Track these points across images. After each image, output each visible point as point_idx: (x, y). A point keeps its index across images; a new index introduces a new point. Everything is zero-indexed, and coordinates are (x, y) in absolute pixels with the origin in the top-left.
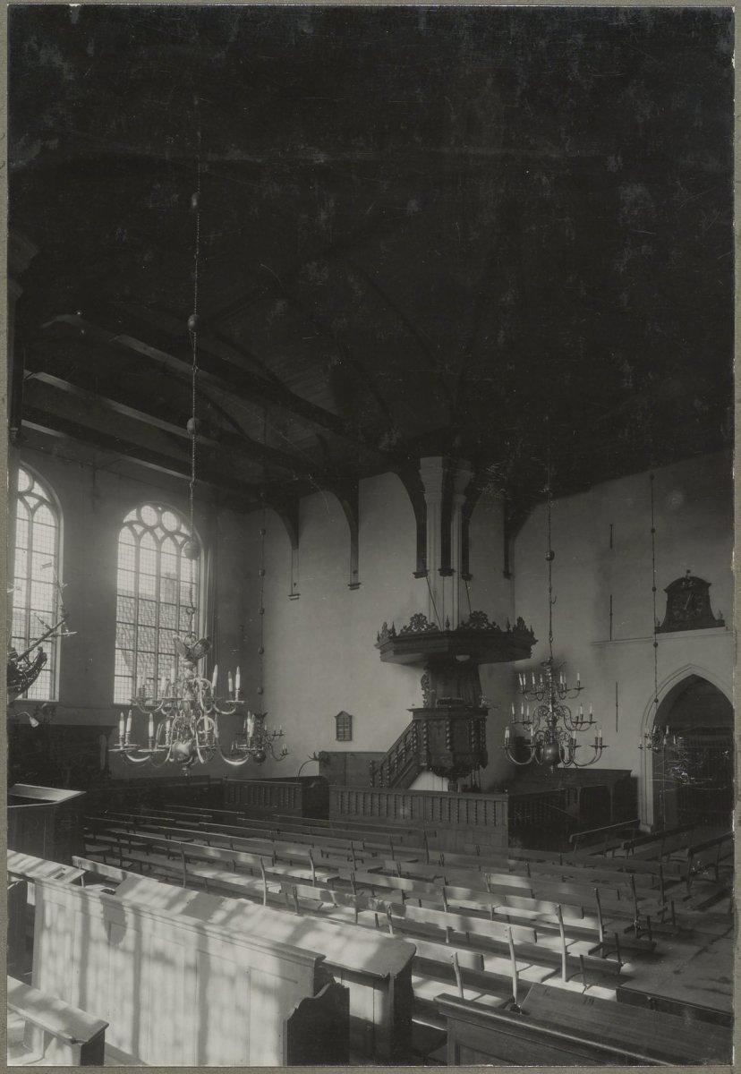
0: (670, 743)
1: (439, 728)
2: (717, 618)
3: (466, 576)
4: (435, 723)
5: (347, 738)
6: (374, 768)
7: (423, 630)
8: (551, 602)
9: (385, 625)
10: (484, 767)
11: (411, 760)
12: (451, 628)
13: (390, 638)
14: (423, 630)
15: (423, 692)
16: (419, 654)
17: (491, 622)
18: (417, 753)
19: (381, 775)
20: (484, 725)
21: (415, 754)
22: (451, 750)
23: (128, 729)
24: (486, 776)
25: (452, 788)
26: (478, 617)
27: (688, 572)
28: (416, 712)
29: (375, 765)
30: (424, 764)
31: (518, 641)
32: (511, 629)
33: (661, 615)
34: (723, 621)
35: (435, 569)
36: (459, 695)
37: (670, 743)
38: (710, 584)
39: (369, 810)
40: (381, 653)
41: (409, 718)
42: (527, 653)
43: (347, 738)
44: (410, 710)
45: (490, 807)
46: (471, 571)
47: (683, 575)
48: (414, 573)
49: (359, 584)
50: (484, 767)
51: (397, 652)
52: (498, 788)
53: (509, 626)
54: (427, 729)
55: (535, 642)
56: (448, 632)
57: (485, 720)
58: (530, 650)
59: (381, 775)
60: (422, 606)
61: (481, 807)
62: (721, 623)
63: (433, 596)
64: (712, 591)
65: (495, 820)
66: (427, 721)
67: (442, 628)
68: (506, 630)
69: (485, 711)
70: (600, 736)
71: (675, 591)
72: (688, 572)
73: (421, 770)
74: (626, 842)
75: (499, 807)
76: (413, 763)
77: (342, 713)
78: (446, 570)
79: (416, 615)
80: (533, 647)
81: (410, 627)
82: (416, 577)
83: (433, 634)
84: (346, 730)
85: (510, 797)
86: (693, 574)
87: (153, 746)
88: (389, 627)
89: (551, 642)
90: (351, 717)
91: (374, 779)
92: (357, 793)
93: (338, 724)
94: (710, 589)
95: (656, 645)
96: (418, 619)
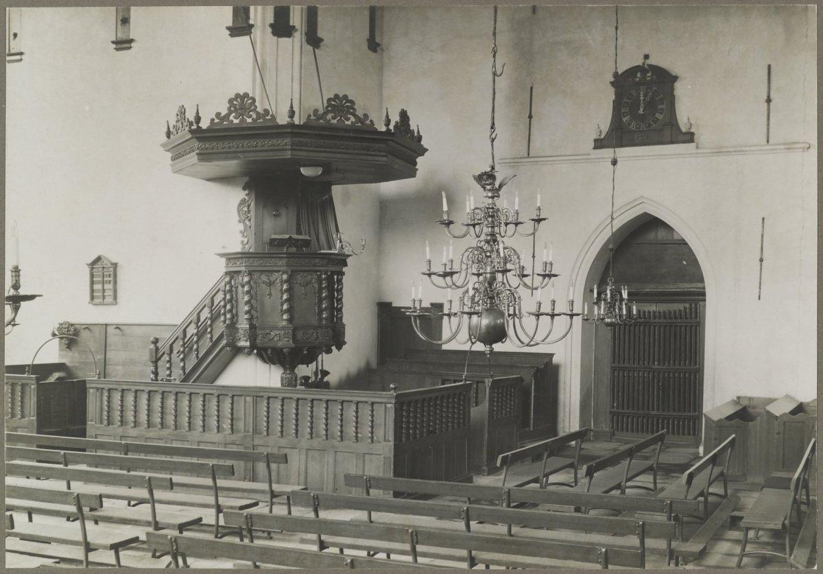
0: (629, 310)
1: (270, 284)
2: (684, 130)
3: (313, 40)
4: (264, 278)
5: (109, 299)
6: (157, 349)
7: (249, 120)
8: (495, 74)
9: (182, 111)
10: (339, 348)
11: (221, 337)
12: (296, 121)
13: (191, 131)
14: (249, 120)
15: (241, 227)
16: (235, 162)
17: (360, 113)
18: (232, 326)
19: (169, 361)
20: (340, 281)
21: (228, 327)
22: (290, 320)
23: (468, 203)
24: (338, 364)
25: (290, 382)
26: (340, 105)
27: (646, 57)
28: (230, 258)
29: (159, 345)
30: (244, 343)
31: (398, 149)
32: (391, 127)
33: (605, 125)
34: (692, 134)
35: (264, 26)
36: (299, 232)
37: (629, 310)
38: (675, 78)
39: (157, 419)
40: (173, 159)
41: (220, 267)
42: (409, 170)
43: (109, 299)
44: (222, 255)
45: (365, 411)
46: (321, 33)
47: (639, 62)
48: (228, 28)
49: (131, 41)
50: (339, 348)
51: (204, 156)
52: (359, 381)
53: (388, 122)
54: (251, 288)
55: (423, 151)
56: (292, 125)
57: (343, 274)
58: (415, 164)
59: (169, 361)
60: (243, 82)
61: (350, 413)
62: (689, 137)
63: (260, 68)
64: (680, 89)
65: (357, 433)
66: (250, 274)
67: (283, 119)
68: (384, 129)
69: (342, 260)
70: (420, 297)
71: (625, 83)
72: (646, 57)
73: (237, 351)
74: (590, 464)
75: (380, 410)
76: (224, 342)
77: (99, 259)
78: (281, 28)
79: (237, 96)
80: (419, 160)
81: (228, 115)
82: (232, 35)
83: (267, 130)
84: (106, 286)
85: (397, 397)
86: (652, 61)
87: (628, 408)
88: (190, 116)
89: (493, 140)
90: (115, 265)
91: (156, 368)
92: (177, 394)
93: (92, 276)
94: (677, 85)
95: (614, 162)
96: (241, 103)
